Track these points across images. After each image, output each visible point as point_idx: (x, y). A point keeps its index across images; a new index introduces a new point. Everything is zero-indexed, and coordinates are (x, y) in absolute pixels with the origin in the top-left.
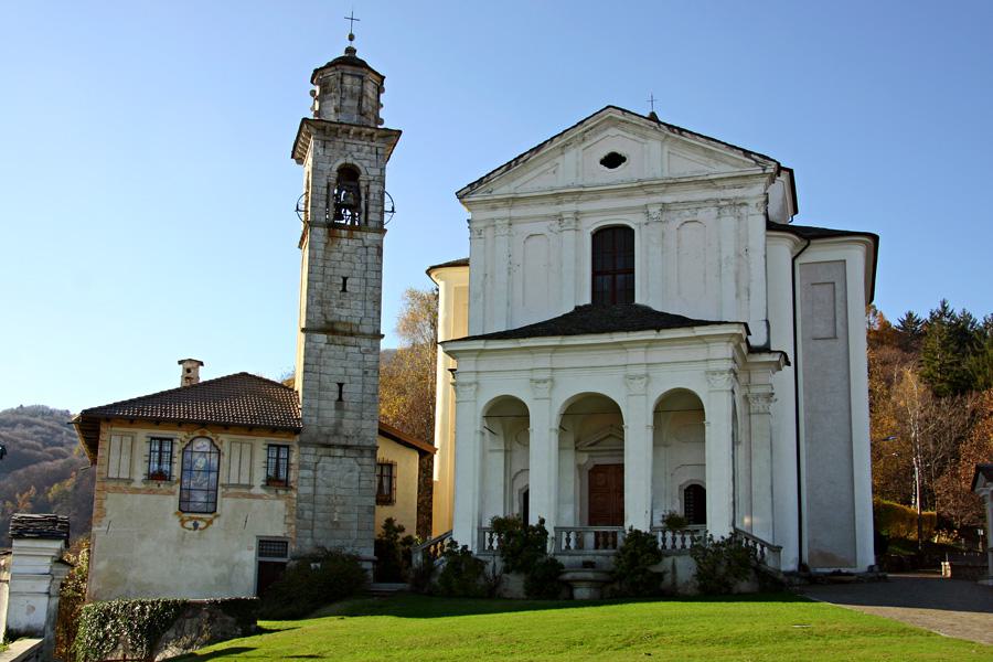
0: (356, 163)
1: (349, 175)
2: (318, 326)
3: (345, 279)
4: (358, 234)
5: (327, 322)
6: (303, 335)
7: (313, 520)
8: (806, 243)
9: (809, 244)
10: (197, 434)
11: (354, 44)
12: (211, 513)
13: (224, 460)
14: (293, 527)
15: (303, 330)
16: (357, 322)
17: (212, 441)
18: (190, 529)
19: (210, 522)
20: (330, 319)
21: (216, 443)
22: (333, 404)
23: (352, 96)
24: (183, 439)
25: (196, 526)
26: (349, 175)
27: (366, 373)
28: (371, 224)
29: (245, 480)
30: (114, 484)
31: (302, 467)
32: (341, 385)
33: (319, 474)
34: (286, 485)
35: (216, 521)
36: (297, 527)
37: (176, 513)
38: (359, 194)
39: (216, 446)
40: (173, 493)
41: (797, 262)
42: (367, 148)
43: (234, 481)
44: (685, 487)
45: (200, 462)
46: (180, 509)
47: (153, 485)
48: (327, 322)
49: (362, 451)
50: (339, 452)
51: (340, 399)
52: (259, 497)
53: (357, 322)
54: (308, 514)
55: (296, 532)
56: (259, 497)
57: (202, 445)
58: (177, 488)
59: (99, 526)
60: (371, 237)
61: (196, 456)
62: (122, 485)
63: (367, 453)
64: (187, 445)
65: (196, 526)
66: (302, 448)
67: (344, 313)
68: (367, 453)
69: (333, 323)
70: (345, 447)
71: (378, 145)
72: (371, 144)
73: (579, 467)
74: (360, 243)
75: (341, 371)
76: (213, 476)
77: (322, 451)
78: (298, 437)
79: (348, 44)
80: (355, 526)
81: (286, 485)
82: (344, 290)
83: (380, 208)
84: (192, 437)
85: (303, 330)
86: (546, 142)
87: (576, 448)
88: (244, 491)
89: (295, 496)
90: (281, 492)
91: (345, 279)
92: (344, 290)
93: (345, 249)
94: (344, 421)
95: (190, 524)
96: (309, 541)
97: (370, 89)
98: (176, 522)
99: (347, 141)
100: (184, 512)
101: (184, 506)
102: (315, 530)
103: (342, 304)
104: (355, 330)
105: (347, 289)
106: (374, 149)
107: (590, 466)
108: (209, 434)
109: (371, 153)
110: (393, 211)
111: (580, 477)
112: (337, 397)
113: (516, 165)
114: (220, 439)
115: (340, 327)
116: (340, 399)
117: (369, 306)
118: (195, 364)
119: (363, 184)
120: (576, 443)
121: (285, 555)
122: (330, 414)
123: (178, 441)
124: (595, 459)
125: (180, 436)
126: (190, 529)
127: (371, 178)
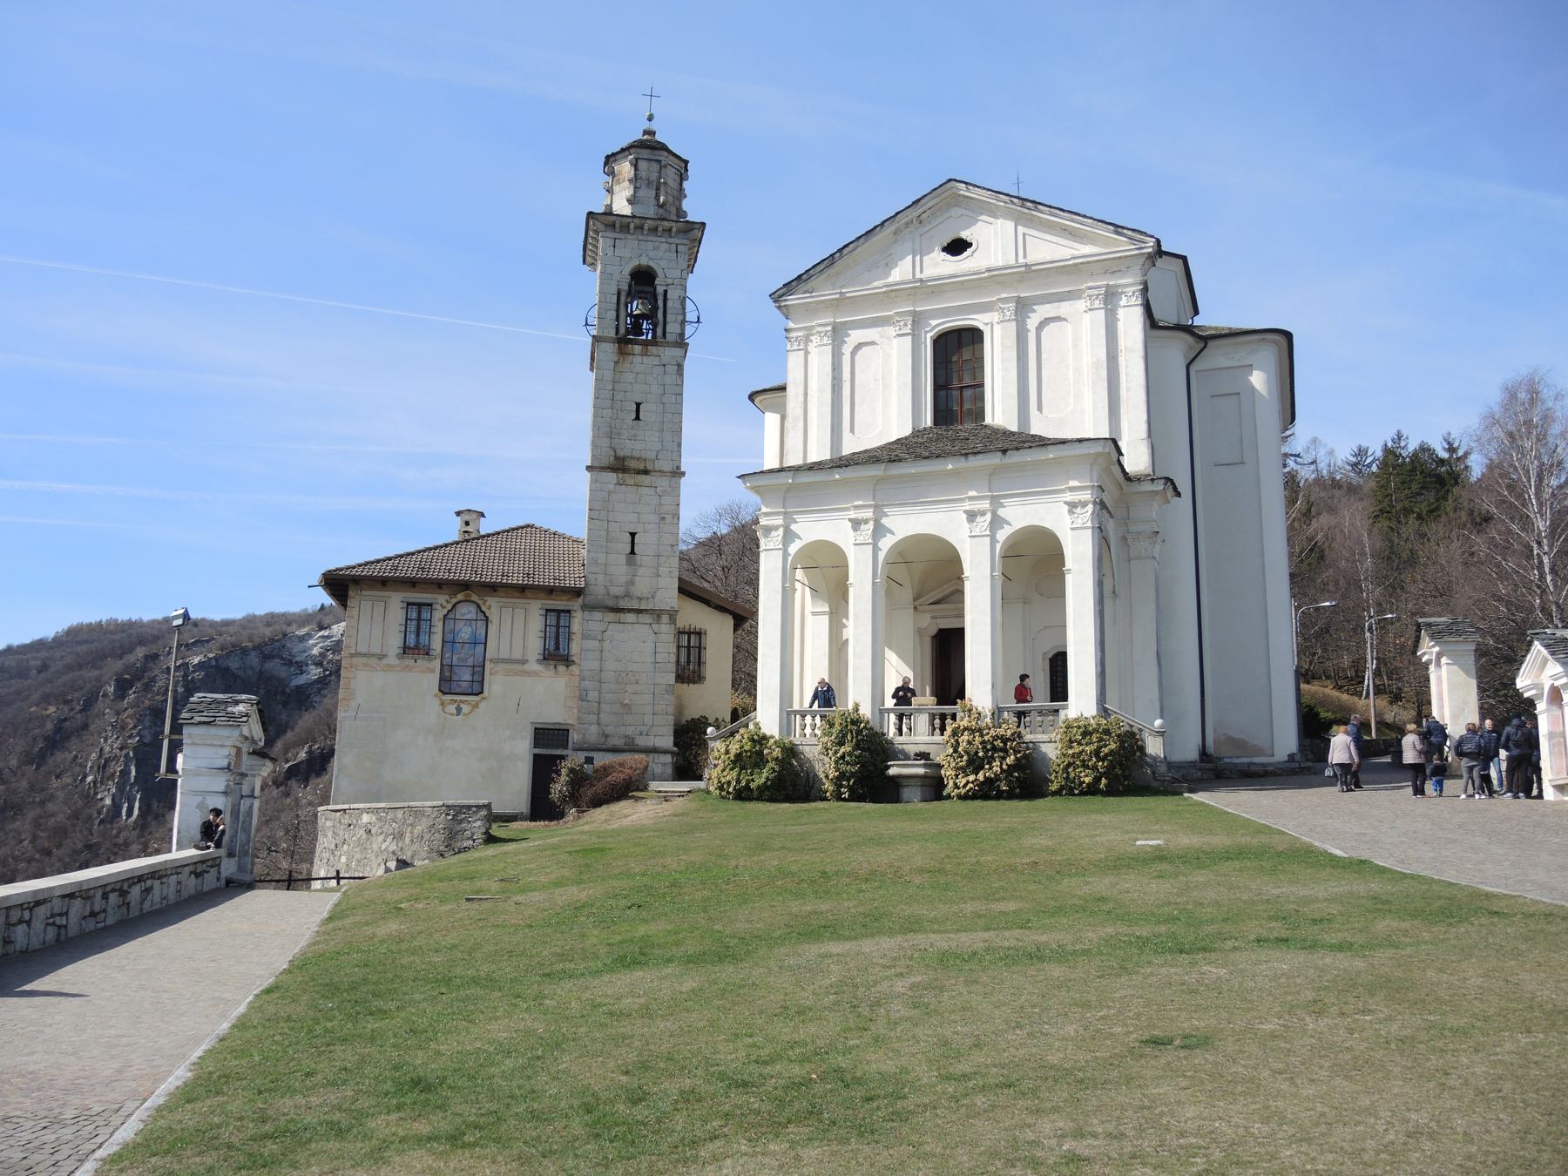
0: (651, 264)
1: (643, 279)
2: (605, 462)
3: (638, 405)
4: (653, 349)
5: (616, 458)
6: (588, 475)
7: (599, 703)
8: (1202, 345)
9: (1205, 346)
10: (460, 597)
11: (654, 126)
12: (477, 695)
13: (493, 629)
14: (576, 710)
15: (589, 468)
16: (653, 457)
17: (479, 606)
18: (452, 715)
19: (476, 706)
20: (621, 453)
21: (484, 609)
22: (623, 559)
23: (649, 184)
24: (445, 604)
25: (459, 710)
26: (643, 279)
27: (663, 518)
28: (670, 337)
29: (517, 655)
30: (364, 660)
31: (585, 637)
32: (633, 535)
33: (607, 645)
34: (567, 661)
35: (482, 705)
36: (579, 711)
37: (436, 695)
38: (656, 301)
39: (484, 613)
40: (432, 671)
41: (1193, 369)
42: (665, 246)
43: (504, 654)
44: (1050, 655)
45: (465, 633)
46: (440, 691)
47: (409, 662)
48: (616, 458)
49: (659, 616)
50: (631, 617)
51: (632, 552)
52: (535, 674)
53: (653, 457)
54: (593, 695)
55: (579, 718)
56: (535, 674)
57: (467, 611)
58: (437, 664)
59: (346, 711)
60: (669, 353)
61: (460, 625)
62: (374, 661)
63: (665, 618)
64: (449, 611)
65: (459, 710)
66: (586, 613)
67: (639, 446)
68: (665, 618)
69: (623, 459)
70: (639, 611)
71: (678, 242)
72: (669, 240)
73: (920, 632)
74: (656, 361)
75: (633, 517)
76: (480, 648)
77: (611, 616)
78: (580, 600)
79: (646, 125)
80: (649, 709)
81: (567, 661)
82: (638, 418)
83: (681, 317)
84: (454, 601)
85: (589, 468)
86: (875, 227)
87: (915, 608)
88: (517, 667)
89: (577, 672)
90: (562, 668)
91: (638, 405)
92: (638, 418)
93: (639, 368)
94: (637, 579)
95: (452, 708)
96: (594, 729)
97: (670, 176)
98: (437, 702)
99: (641, 237)
100: (444, 693)
101: (447, 685)
102: (601, 715)
103: (635, 435)
104: (650, 467)
105: (641, 417)
106: (674, 247)
107: (934, 632)
108: (474, 598)
109: (670, 251)
110: (698, 321)
111: (921, 643)
112: (628, 550)
113: (841, 257)
114: (487, 604)
115: (632, 464)
116: (632, 552)
117: (667, 436)
118: (475, 516)
119: (660, 290)
120: (915, 599)
121: (565, 747)
122: (620, 569)
123: (438, 607)
124: (939, 621)
125: (441, 600)
126: (452, 715)
127: (670, 281)
